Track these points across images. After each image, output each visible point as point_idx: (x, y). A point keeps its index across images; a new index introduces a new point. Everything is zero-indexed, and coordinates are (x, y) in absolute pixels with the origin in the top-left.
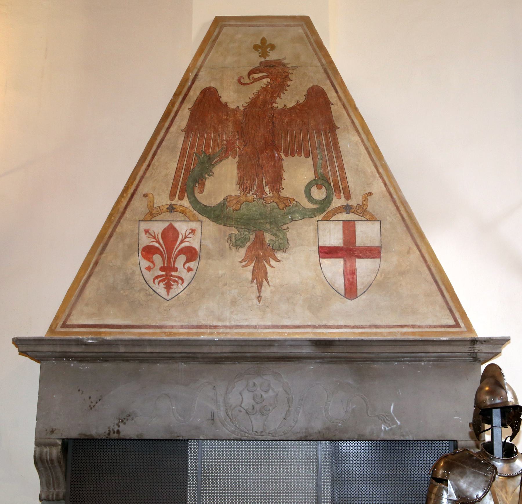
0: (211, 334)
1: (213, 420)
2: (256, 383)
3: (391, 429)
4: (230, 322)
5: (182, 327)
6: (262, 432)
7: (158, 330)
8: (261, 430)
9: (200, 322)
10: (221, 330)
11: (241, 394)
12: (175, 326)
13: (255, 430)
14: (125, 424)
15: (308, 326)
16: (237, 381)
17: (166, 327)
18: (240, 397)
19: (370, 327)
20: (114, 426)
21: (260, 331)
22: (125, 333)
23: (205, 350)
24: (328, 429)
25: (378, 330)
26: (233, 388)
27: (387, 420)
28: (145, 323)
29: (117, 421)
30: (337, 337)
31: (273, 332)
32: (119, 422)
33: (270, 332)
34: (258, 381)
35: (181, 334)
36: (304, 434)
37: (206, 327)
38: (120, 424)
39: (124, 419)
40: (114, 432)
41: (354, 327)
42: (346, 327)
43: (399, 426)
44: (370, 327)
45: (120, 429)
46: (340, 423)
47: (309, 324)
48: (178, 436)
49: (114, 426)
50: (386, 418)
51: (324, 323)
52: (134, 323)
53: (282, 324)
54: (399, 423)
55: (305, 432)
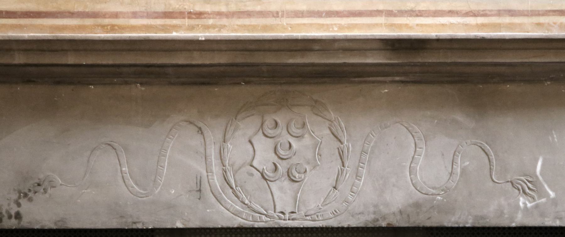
0: (191, 28)
1: (200, 190)
2: (279, 121)
3: (537, 206)
4: (227, 5)
5: (135, 15)
6: (293, 212)
7: (88, 22)
8: (288, 209)
9: (170, 5)
10: (211, 22)
11: (250, 142)
12: (121, 13)
13: (278, 209)
14: (30, 200)
15: (379, 13)
16: (244, 119)
17: (104, 15)
18: (249, 146)
19: (499, 13)
20: (9, 205)
21: (285, 21)
22: (25, 26)
23: (181, 60)
24: (417, 205)
25: (517, 20)
26: (235, 130)
27: (529, 188)
28: (63, 8)
29: (15, 196)
30: (433, 34)
31: (311, 25)
32: (19, 197)
33: (304, 24)
34: (281, 118)
35: (133, 28)
36: (373, 216)
37: (181, 14)
38: (20, 201)
39: (30, 190)
40: (10, 217)
41: (468, 14)
42: (451, 13)
43: (553, 199)
44: (499, 13)
45: (22, 210)
46: (439, 195)
47: (381, 7)
48: (135, 223)
49: (9, 205)
50: (530, 186)
51: (410, 6)
52: (42, 8)
53: (327, 8)
54: (552, 194)
55: (374, 213)
